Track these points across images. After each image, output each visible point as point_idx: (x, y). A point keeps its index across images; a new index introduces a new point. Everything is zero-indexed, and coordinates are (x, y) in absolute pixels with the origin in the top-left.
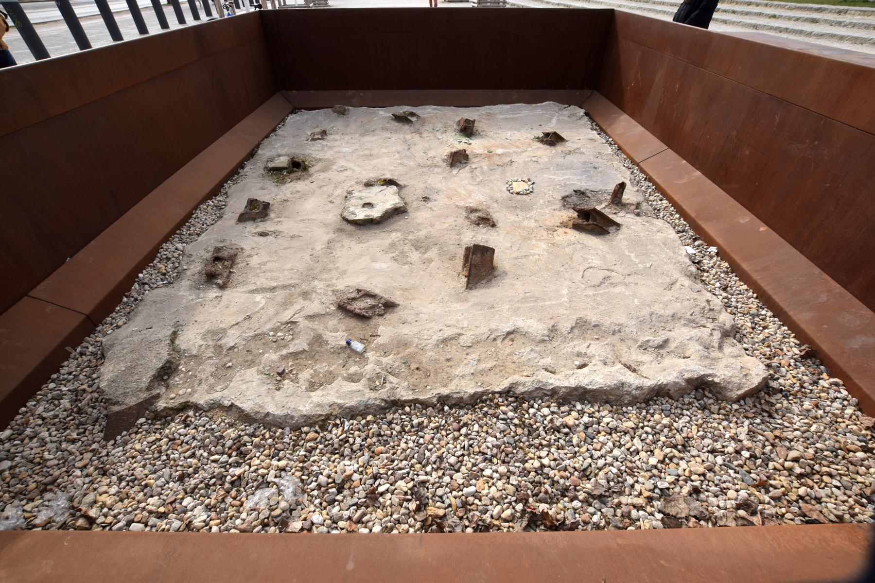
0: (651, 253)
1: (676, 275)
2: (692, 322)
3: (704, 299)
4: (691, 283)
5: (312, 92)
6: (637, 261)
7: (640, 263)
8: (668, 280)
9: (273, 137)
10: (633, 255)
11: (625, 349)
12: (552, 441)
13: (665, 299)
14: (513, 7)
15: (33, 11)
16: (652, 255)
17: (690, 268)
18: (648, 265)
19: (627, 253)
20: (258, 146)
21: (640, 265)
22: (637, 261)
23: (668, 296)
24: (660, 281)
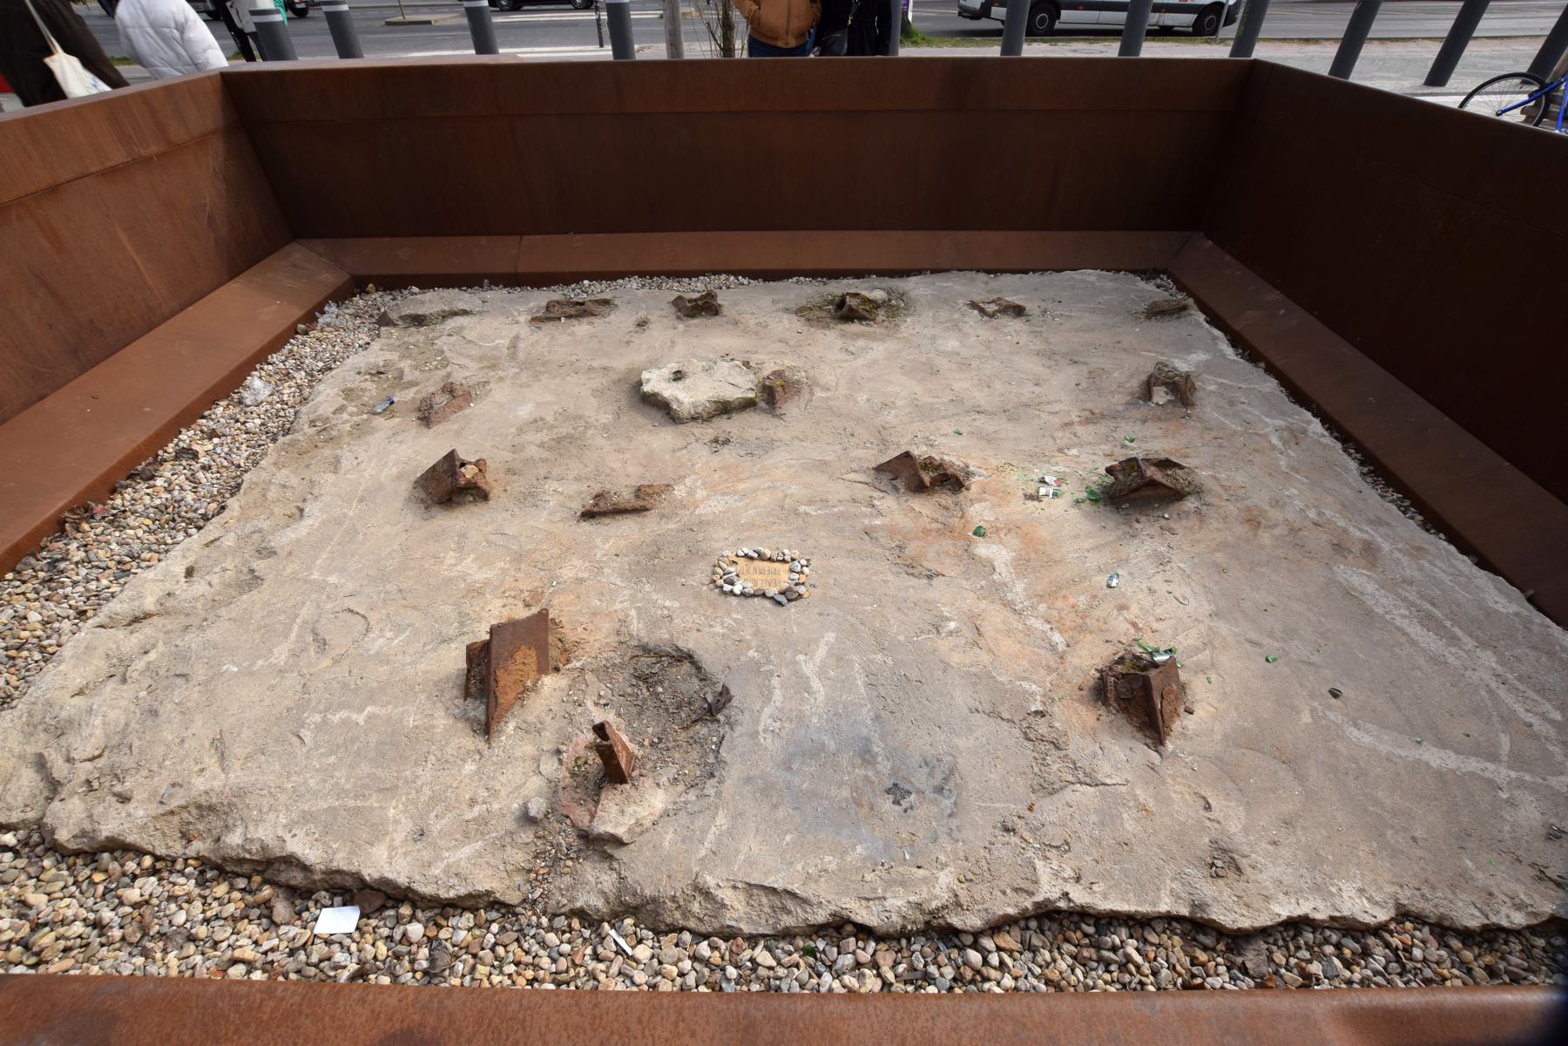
0: (341, 759)
1: (237, 776)
2: (118, 742)
3: (139, 795)
4: (194, 793)
5: (1228, 258)
6: (336, 718)
7: (325, 721)
8: (238, 750)
9: (982, 276)
10: (360, 719)
11: (169, 627)
12: (495, 927)
13: (199, 720)
14: (1012, 288)
15: (1424, 16)
16: (332, 759)
17: (240, 830)
18: (307, 735)
19: (369, 709)
20: (919, 272)
21: (317, 718)
22: (336, 718)
23: (201, 728)
24: (246, 733)
